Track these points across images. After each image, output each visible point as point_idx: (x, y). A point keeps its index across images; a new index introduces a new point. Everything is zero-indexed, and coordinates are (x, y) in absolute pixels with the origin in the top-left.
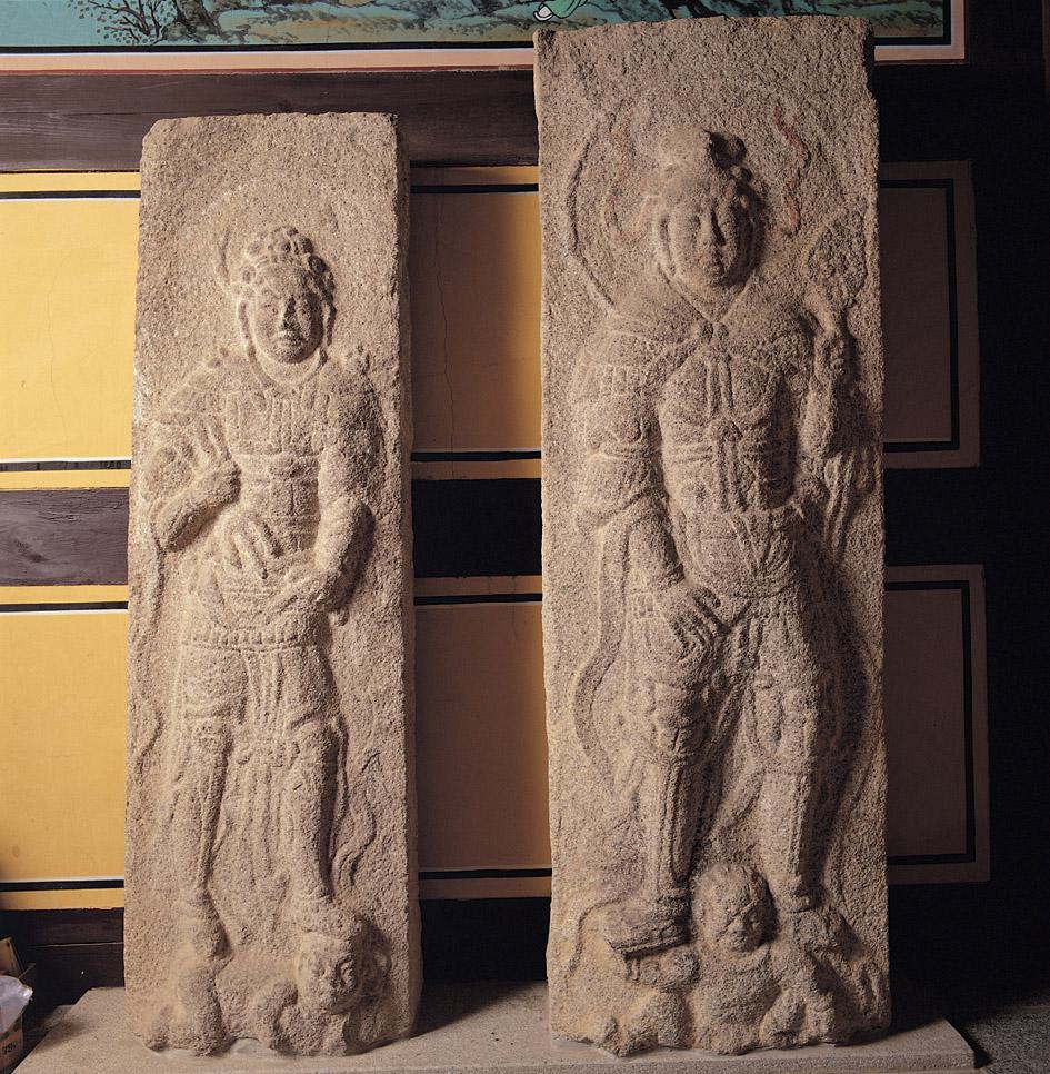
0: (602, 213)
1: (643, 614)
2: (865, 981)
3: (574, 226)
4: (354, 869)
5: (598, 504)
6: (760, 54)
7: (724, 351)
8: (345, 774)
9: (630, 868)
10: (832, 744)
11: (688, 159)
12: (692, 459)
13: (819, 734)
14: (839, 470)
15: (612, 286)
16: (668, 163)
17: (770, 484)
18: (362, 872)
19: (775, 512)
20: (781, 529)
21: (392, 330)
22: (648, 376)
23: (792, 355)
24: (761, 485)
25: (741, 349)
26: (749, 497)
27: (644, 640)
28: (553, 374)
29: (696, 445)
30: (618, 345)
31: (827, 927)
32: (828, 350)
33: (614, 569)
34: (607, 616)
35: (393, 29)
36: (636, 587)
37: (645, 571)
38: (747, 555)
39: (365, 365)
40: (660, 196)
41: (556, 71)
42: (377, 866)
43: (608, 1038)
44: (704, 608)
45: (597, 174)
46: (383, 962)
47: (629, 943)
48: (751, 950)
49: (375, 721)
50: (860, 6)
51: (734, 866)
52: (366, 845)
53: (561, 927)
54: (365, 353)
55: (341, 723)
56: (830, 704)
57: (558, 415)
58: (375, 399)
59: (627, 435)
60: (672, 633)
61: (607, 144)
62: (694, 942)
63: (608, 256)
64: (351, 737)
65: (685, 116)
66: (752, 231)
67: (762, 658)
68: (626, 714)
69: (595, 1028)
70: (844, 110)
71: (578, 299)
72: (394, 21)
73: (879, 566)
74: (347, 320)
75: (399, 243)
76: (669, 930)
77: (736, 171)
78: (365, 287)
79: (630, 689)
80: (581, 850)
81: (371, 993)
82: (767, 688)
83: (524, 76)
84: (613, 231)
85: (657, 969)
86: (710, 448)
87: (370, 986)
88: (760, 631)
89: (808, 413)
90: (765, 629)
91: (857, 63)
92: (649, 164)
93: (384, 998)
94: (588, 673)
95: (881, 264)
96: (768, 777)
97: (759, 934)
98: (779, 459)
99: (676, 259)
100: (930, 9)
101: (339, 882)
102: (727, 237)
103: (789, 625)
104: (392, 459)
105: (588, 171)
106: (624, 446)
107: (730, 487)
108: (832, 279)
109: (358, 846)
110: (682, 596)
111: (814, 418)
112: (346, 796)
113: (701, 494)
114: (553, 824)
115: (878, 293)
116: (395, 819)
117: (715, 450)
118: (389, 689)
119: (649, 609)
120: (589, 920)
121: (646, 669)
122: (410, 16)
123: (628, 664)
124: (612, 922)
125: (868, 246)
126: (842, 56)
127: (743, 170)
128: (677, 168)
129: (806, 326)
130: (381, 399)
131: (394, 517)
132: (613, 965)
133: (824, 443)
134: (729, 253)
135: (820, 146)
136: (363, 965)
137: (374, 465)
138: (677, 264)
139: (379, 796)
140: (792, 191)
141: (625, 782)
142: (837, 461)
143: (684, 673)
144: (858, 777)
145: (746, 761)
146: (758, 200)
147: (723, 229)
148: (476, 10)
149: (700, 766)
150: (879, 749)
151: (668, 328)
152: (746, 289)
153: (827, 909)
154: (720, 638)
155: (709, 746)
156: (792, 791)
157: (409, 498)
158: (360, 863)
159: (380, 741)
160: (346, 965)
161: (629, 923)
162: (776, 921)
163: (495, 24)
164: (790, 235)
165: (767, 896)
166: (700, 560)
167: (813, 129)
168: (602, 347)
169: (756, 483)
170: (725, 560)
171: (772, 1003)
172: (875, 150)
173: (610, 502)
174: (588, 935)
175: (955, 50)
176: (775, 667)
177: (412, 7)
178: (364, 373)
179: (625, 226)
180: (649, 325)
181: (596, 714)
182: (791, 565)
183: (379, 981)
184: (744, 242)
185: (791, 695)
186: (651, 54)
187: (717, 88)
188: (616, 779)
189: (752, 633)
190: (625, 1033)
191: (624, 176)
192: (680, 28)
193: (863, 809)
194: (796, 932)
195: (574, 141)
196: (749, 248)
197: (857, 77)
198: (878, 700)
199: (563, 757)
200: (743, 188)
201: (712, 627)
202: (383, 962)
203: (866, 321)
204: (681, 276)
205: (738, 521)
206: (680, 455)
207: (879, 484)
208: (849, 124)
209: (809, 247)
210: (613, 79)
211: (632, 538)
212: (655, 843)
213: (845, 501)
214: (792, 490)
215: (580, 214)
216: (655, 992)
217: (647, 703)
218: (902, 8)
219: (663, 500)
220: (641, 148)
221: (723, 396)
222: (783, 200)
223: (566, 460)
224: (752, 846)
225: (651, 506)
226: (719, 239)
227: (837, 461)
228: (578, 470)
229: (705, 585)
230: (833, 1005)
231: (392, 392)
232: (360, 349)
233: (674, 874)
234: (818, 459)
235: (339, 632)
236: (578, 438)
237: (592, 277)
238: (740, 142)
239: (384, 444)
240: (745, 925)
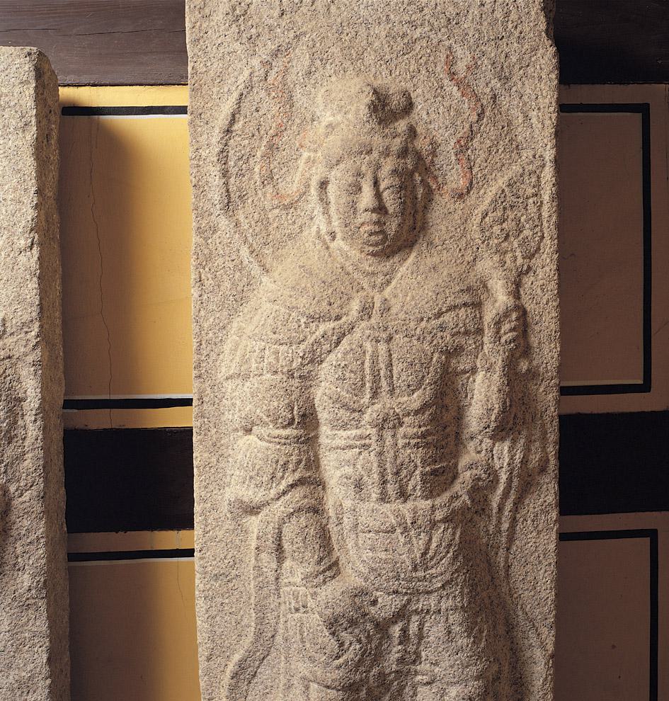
1: (297, 610)
11: (350, 116)
12: (351, 447)
14: (509, 451)
16: (327, 118)
19: (438, 501)
22: (302, 358)
24: (423, 474)
26: (410, 487)
27: (299, 637)
28: (204, 346)
29: (354, 432)
30: (270, 321)
33: (268, 560)
34: (261, 609)
36: (291, 580)
45: (251, 129)
59: (280, 421)
61: (263, 94)
63: (264, 222)
67: (423, 654)
75: (39, 192)
79: (285, 685)
82: (428, 683)
89: (476, 392)
92: (309, 117)
94: (242, 666)
95: (560, 226)
103: (451, 621)
105: (241, 123)
107: (389, 477)
108: (506, 244)
111: (482, 394)
113: (359, 486)
123: (283, 658)
125: (545, 208)
131: (35, 494)
133: (493, 425)
134: (392, 226)
138: (337, 230)
142: (506, 445)
143: (337, 674)
154: (378, 636)
157: (59, 461)
166: (359, 556)
169: (417, 472)
170: (383, 555)
172: (554, 104)
176: (436, 664)
184: (403, 223)
187: (383, 34)
189: (413, 628)
195: (226, 90)
209: (482, 208)
210: (270, 22)
211: (285, 530)
213: (516, 482)
221: (383, 379)
222: (453, 158)
226: (380, 209)
228: (231, 452)
236: (230, 417)
238: (406, 94)
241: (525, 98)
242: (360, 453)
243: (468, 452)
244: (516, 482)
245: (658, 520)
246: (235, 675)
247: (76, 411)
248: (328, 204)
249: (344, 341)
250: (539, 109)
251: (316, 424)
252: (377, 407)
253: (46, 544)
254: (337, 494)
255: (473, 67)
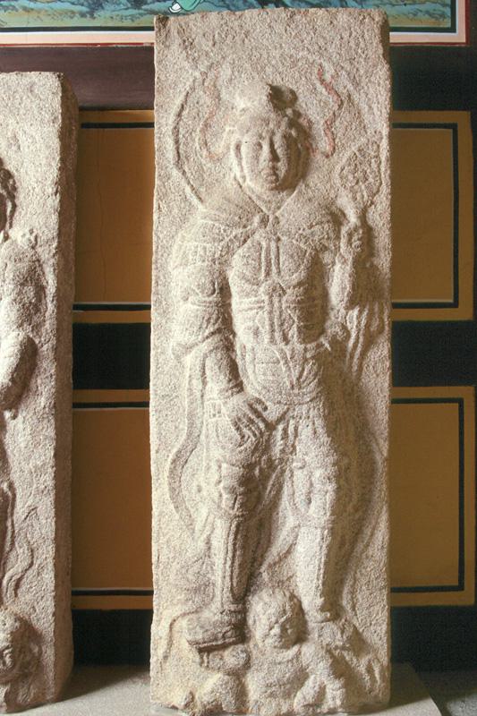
0: (197, 140)
1: (214, 415)
2: (370, 670)
3: (178, 149)
4: (17, 586)
5: (187, 338)
6: (308, 33)
7: (276, 234)
8: (13, 521)
9: (205, 590)
10: (350, 508)
11: (255, 103)
12: (251, 309)
13: (338, 500)
15: (202, 190)
16: (242, 106)
17: (305, 327)
18: (23, 588)
19: (308, 346)
20: (313, 358)
21: (54, 219)
23: (323, 238)
24: (299, 328)
25: (288, 234)
26: (290, 335)
29: (254, 299)
31: (342, 633)
32: (350, 235)
33: (197, 384)
34: (191, 416)
35: (72, 18)
37: (217, 383)
38: (287, 376)
39: (34, 242)
40: (236, 128)
41: (167, 43)
42: (34, 584)
43: (187, 706)
44: (255, 411)
45: (194, 113)
46: (36, 650)
47: (201, 641)
48: (287, 647)
49: (35, 486)
50: (394, 5)
51: (277, 590)
52: (26, 570)
53: (158, 630)
54: (34, 235)
55: (11, 486)
56: (347, 480)
57: (162, 278)
58: (40, 266)
60: (233, 429)
62: (248, 642)
64: (18, 496)
65: (255, 74)
66: (300, 153)
67: (298, 448)
68: (203, 485)
69: (179, 699)
70: (366, 72)
71: (179, 198)
72: (73, 12)
73: (386, 385)
74: (23, 212)
76: (229, 633)
77: (289, 112)
78: (37, 190)
80: (172, 578)
81: (26, 671)
82: (301, 468)
83: (149, 50)
84: (205, 153)
85: (221, 659)
86: (263, 301)
87: (24, 666)
88: (296, 429)
90: (300, 428)
91: (376, 40)
93: (36, 674)
96: (303, 530)
97: (293, 637)
98: (313, 310)
99: (246, 171)
100: (442, 9)
101: (6, 595)
102: (281, 156)
103: (316, 425)
104: (50, 307)
106: (204, 299)
109: (20, 570)
110: (241, 404)
111: (339, 282)
112: (13, 537)
113: (256, 333)
114: (154, 559)
115: (390, 197)
116: (47, 553)
117: (266, 303)
118: (44, 464)
119: (219, 410)
120: (177, 626)
121: (217, 453)
122: (84, 9)
124: (191, 626)
125: (383, 164)
126: (366, 36)
127: (294, 111)
128: (248, 109)
129: (337, 218)
130: (44, 265)
131: (51, 346)
132: (191, 656)
133: (346, 299)
134: (282, 167)
135: (349, 96)
136: (20, 651)
137: (37, 310)
138: (247, 175)
139: (36, 536)
140: (329, 125)
141: (202, 531)
142: (355, 312)
144: (368, 531)
145: (288, 518)
146: (305, 132)
147: (278, 151)
148: (129, 5)
149: (254, 521)
150: (383, 513)
151: (237, 218)
152: (295, 192)
153: (343, 620)
155: (260, 507)
156: (318, 540)
158: (22, 582)
159: (37, 500)
160: (7, 651)
161: (202, 627)
162: (306, 628)
163: (141, 15)
164: (327, 157)
165: (299, 611)
166: (256, 379)
167: (344, 85)
168: (192, 231)
169: (295, 326)
171: (302, 684)
173: (193, 337)
174: (176, 635)
175: (459, 36)
177: (85, 3)
178: (33, 248)
179: (212, 149)
180: (224, 216)
181: (184, 484)
182: (319, 383)
183: (32, 663)
184: (294, 157)
185: (318, 473)
186: (233, 33)
187: (278, 56)
188: (196, 529)
189: (291, 430)
190: (199, 703)
191: (212, 115)
192: (252, 16)
193: (371, 553)
194: (320, 636)
196: (298, 165)
197: (376, 50)
198: (384, 479)
199: (161, 514)
200: (293, 123)
201: (262, 426)
202: (36, 650)
203: (380, 216)
204: (250, 183)
205: (282, 351)
206: (243, 306)
207: (387, 328)
208: (370, 81)
212: (220, 573)
213: (361, 340)
214: (323, 332)
215: (182, 140)
216: (220, 675)
217: (216, 477)
218: (423, 7)
219: (231, 337)
220: (224, 95)
223: (167, 308)
224: (291, 577)
225: (221, 340)
226: (275, 157)
227: (355, 312)
229: (257, 395)
230: (345, 686)
231: (52, 261)
232: (31, 232)
233: (233, 595)
234: (343, 311)
235: (11, 424)
237: (189, 183)
238: (292, 92)
239: (45, 297)
240: (282, 631)
241: (369, 96)
242: (257, 313)
243: (330, 318)
244: (361, 340)
245: (467, 393)
246: (174, 461)
247: (82, 311)
248: (241, 159)
249: (249, 241)
250: (378, 103)
251: (230, 296)
252: (270, 282)
253: (56, 380)
254: (243, 336)
255: (336, 76)
